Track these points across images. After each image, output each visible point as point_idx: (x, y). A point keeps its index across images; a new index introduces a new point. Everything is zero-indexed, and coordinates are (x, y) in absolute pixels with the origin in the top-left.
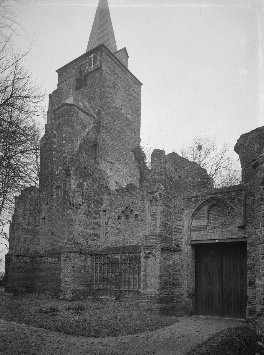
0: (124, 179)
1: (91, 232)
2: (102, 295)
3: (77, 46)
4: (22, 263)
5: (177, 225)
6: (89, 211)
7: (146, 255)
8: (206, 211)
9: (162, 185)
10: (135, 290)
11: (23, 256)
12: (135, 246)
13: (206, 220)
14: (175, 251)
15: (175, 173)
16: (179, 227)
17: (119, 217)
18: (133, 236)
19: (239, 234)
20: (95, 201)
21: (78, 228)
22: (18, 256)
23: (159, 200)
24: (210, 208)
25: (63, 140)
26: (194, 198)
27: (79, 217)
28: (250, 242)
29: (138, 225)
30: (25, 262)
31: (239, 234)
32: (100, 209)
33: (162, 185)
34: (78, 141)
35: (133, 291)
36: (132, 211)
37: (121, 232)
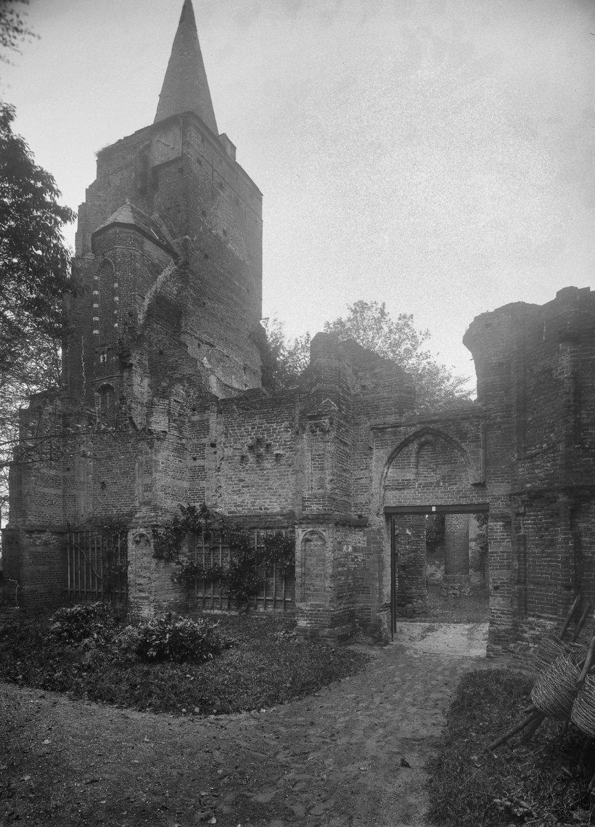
0: (233, 377)
1: (186, 485)
2: (212, 608)
3: (136, 108)
4: (38, 546)
5: (358, 476)
6: (183, 445)
7: (306, 534)
8: (414, 452)
9: (333, 403)
10: (279, 598)
11: (40, 532)
12: (278, 515)
13: (414, 470)
14: (356, 527)
15: (355, 378)
16: (363, 481)
17: (243, 457)
18: (273, 495)
19: (474, 497)
20: (193, 424)
21: (162, 480)
22: (30, 532)
23: (328, 431)
24: (421, 446)
25: (114, 295)
26: (390, 428)
27: (164, 456)
28: (494, 512)
29: (282, 475)
30: (46, 544)
31: (474, 497)
32: (204, 441)
33: (333, 403)
34: (144, 299)
35: (276, 601)
36: (268, 446)
37: (247, 486)
